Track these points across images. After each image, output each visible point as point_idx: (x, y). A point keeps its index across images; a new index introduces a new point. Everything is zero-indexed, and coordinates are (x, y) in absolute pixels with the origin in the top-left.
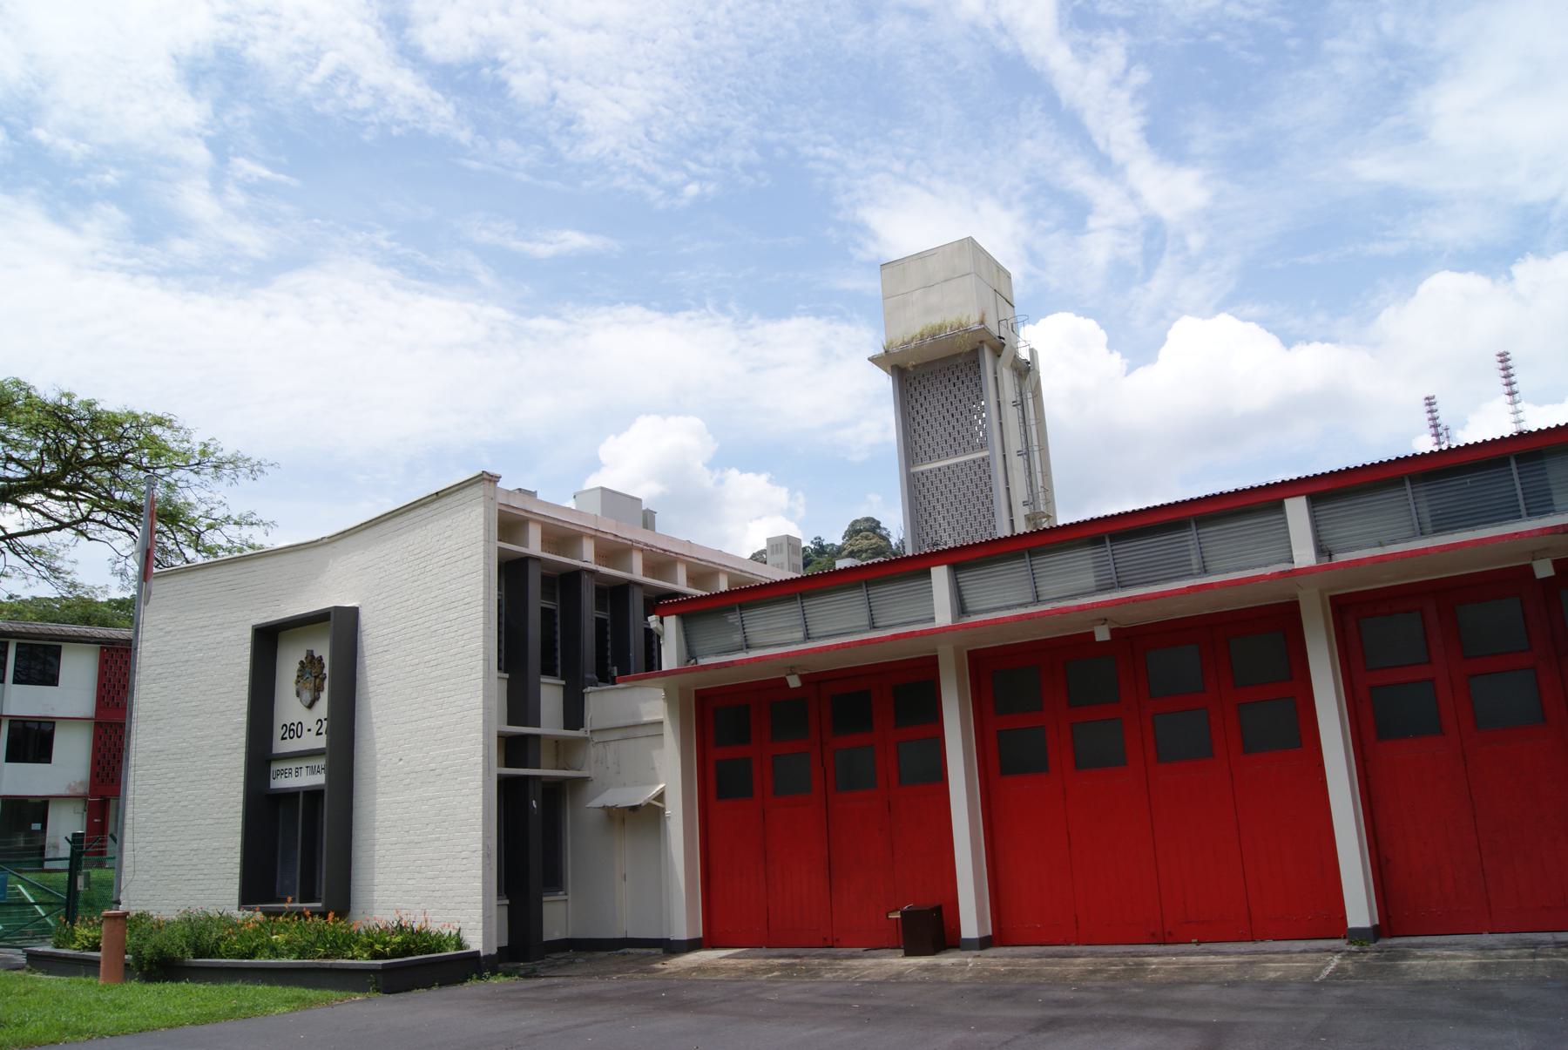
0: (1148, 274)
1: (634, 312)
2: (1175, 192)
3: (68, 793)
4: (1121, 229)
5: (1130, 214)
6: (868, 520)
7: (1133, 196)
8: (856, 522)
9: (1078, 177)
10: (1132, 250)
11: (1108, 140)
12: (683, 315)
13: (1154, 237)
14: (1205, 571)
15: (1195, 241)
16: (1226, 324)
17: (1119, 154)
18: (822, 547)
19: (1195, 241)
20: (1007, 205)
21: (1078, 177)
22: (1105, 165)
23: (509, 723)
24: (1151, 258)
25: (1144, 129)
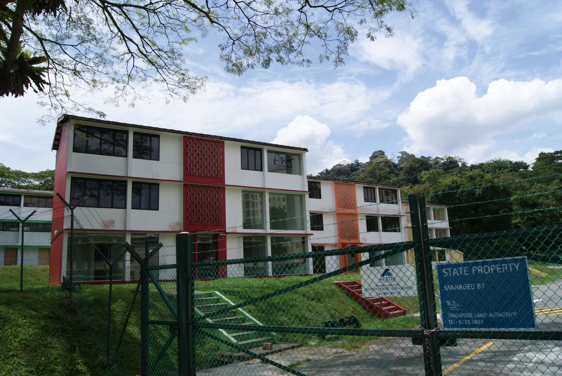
0: (470, 63)
1: (278, 84)
2: (480, 29)
3: (170, 230)
4: (459, 46)
5: (462, 39)
6: (379, 151)
7: (464, 32)
8: (375, 152)
9: (443, 26)
10: (464, 53)
11: (454, 12)
12: (297, 84)
13: (472, 46)
14: (443, 295)
15: (487, 49)
16: (502, 82)
17: (459, 16)
18: (358, 163)
19: (487, 49)
20: (415, 38)
21: (443, 26)
22: (454, 21)
23: (245, 227)
24: (471, 56)
25: (468, 5)
